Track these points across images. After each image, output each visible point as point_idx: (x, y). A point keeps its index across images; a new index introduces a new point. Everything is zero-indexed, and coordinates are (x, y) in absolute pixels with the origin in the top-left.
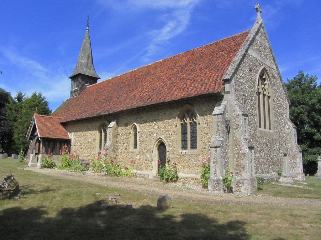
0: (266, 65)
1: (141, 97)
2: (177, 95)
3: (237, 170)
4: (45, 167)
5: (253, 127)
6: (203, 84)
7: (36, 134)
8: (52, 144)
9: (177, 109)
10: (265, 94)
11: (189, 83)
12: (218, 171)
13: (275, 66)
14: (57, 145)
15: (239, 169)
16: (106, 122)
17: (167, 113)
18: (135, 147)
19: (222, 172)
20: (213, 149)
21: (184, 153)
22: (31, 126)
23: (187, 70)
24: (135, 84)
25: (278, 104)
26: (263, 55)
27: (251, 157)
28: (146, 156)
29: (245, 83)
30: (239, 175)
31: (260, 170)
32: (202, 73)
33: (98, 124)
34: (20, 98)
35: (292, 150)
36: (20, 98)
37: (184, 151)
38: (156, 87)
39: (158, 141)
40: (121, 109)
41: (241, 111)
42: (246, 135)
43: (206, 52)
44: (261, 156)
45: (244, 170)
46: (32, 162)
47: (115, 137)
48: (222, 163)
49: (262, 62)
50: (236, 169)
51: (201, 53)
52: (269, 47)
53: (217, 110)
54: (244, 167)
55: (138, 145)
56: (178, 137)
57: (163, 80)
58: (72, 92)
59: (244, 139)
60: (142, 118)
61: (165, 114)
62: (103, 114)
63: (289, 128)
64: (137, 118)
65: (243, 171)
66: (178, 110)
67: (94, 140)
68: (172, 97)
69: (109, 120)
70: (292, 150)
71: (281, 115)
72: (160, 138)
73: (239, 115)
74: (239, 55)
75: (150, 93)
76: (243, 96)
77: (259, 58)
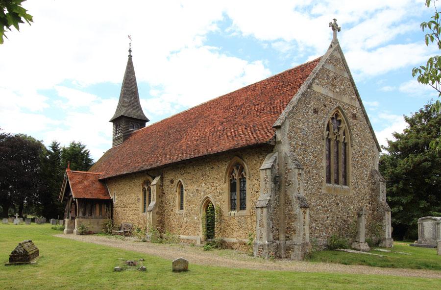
0: (343, 102)
1: (188, 147)
2: (226, 145)
3: (288, 234)
4: (82, 234)
5: (315, 183)
6: (255, 131)
7: (70, 194)
8: (89, 205)
9: (226, 162)
10: (338, 141)
11: (241, 129)
12: (264, 234)
13: (359, 103)
14: (96, 209)
15: (290, 233)
16: (150, 178)
17: (215, 167)
18: (182, 208)
19: (268, 236)
20: (259, 210)
21: (232, 215)
22: (64, 185)
23: (243, 113)
24: (184, 130)
25: (359, 152)
26: (338, 90)
27: (304, 218)
28: (193, 219)
29: (307, 129)
30: (290, 239)
31: (324, 234)
32: (258, 116)
33: (140, 181)
34: (55, 146)
35: (377, 210)
36: (55, 146)
37: (233, 212)
38: (206, 134)
39: (205, 202)
40: (165, 162)
41: (294, 164)
42: (299, 193)
43: (269, 87)
44: (328, 217)
45: (295, 233)
46: (68, 228)
47: (160, 197)
48: (269, 226)
49: (334, 99)
50: (286, 233)
51: (262, 88)
52: (349, 78)
53: (267, 163)
54: (295, 230)
55: (185, 206)
56: (226, 196)
57: (214, 125)
58: (114, 140)
59: (295, 197)
60: (188, 173)
61: (212, 168)
62: (145, 168)
63: (375, 183)
64: (184, 174)
65: (294, 235)
66: (226, 163)
67: (138, 200)
68: (220, 147)
69: (153, 175)
70: (377, 210)
71: (364, 166)
72: (208, 197)
73: (291, 169)
74: (299, 93)
75: (198, 142)
76: (302, 145)
77: (331, 95)
